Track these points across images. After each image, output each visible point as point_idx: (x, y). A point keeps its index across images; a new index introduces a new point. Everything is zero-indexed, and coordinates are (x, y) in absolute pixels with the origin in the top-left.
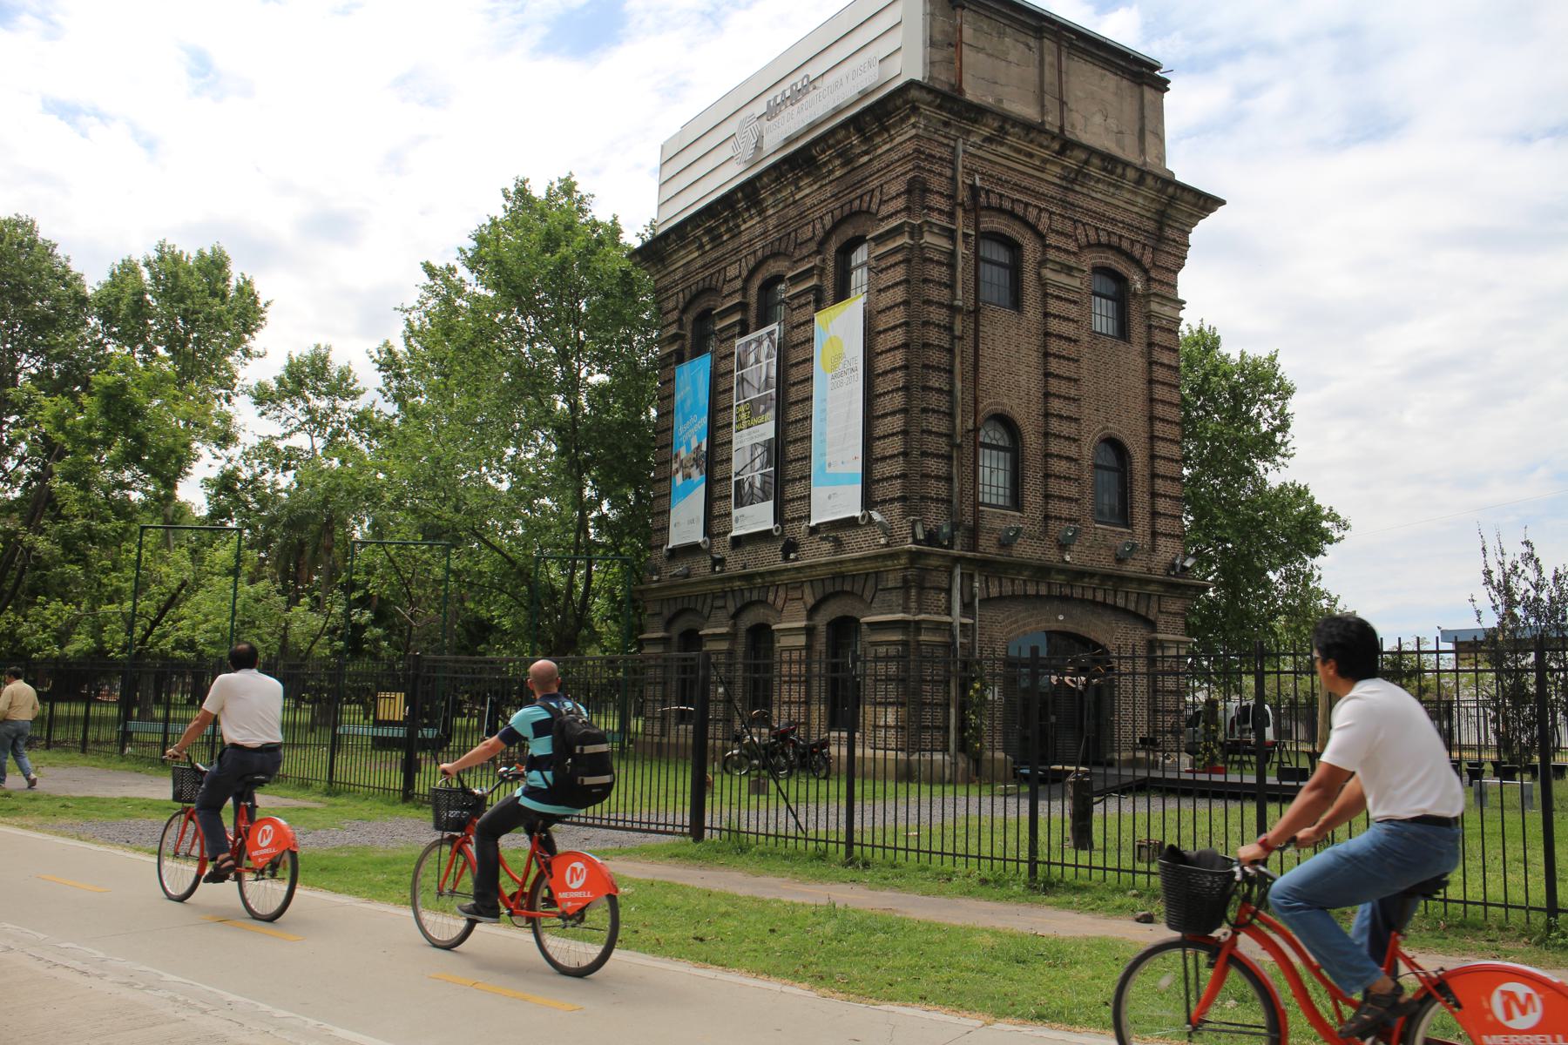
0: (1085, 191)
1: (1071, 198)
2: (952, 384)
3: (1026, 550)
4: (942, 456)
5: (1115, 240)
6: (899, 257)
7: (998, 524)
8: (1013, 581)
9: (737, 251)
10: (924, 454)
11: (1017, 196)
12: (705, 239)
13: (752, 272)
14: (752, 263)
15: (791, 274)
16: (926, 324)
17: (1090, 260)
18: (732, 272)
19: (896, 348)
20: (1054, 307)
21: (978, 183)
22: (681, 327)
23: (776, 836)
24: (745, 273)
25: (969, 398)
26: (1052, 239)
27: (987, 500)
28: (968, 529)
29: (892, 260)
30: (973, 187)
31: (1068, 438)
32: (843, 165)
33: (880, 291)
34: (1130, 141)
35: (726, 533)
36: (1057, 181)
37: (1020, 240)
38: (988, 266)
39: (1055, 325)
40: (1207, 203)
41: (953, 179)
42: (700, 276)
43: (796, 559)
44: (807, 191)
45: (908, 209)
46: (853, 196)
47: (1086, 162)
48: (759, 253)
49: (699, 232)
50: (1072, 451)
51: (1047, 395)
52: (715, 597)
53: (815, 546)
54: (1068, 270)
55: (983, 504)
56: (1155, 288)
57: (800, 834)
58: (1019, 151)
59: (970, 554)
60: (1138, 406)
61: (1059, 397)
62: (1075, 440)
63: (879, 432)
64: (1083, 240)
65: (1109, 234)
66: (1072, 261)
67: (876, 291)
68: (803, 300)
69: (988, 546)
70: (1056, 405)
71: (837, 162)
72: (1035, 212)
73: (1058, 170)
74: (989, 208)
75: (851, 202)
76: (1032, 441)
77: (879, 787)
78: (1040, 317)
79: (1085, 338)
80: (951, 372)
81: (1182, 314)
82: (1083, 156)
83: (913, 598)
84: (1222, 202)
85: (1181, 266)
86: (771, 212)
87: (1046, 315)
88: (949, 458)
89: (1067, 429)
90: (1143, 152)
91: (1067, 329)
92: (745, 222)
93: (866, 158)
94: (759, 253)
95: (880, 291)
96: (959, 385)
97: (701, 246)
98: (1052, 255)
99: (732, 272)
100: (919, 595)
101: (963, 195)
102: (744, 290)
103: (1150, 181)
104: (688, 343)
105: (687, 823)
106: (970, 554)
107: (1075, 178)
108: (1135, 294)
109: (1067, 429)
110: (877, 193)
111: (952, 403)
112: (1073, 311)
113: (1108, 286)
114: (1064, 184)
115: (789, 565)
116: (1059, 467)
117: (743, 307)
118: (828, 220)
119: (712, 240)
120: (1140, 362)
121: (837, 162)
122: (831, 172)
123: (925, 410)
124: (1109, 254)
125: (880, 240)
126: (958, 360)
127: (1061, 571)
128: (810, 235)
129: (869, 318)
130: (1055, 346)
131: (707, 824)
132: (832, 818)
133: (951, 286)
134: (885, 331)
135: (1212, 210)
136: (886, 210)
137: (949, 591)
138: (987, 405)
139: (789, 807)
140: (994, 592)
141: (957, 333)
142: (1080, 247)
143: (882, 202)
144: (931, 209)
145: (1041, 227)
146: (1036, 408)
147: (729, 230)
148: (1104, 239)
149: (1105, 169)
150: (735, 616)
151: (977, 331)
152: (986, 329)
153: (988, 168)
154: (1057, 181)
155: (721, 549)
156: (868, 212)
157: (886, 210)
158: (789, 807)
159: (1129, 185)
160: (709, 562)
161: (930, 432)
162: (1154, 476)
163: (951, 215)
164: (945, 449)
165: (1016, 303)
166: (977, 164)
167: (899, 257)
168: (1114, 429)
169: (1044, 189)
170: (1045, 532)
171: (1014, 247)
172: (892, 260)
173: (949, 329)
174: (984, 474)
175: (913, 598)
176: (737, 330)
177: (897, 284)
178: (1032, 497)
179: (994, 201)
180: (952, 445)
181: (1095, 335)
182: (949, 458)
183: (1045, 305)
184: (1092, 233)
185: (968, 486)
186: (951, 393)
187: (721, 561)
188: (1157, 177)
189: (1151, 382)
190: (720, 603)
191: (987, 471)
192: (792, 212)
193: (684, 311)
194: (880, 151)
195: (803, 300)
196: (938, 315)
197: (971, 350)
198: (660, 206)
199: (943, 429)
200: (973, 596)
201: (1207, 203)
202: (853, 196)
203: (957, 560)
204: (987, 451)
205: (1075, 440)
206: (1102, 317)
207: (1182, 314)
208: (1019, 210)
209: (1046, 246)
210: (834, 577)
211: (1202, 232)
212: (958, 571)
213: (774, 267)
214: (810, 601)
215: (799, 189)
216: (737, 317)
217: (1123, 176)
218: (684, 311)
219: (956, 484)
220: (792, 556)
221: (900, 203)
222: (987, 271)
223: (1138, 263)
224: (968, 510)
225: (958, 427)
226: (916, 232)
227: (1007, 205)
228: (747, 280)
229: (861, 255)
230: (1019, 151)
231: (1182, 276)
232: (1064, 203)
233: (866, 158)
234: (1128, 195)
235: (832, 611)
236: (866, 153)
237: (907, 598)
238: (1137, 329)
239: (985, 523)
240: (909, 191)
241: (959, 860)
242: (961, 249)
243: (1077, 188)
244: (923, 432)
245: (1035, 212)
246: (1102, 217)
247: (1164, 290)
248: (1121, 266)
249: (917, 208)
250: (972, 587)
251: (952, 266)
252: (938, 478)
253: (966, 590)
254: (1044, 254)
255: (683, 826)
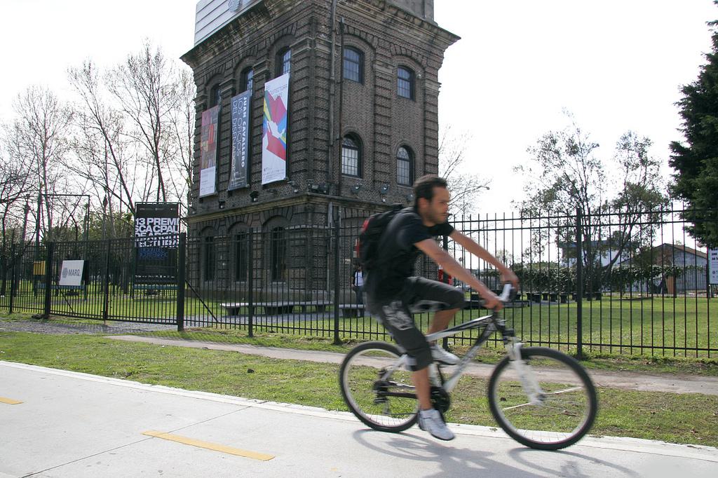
0: (395, 28)
1: (388, 31)
2: (329, 116)
3: (364, 197)
4: (324, 151)
5: (409, 53)
6: (304, 55)
7: (351, 183)
8: (358, 210)
9: (230, 55)
10: (315, 149)
11: (362, 29)
12: (216, 49)
13: (238, 65)
14: (237, 61)
15: (255, 65)
16: (317, 87)
17: (397, 61)
18: (229, 65)
19: (302, 99)
20: (379, 82)
21: (343, 21)
22: (205, 92)
23: (221, 323)
24: (234, 65)
25: (337, 124)
26: (379, 51)
27: (346, 172)
28: (336, 186)
29: (301, 57)
30: (340, 23)
31: (385, 144)
32: (280, 11)
33: (295, 72)
34: (418, 8)
35: (225, 190)
36: (382, 23)
37: (364, 50)
38: (348, 62)
39: (379, 91)
40: (453, 38)
41: (331, 19)
42: (213, 68)
43: (257, 201)
44: (263, 25)
45: (309, 32)
46: (284, 26)
47: (396, 15)
48: (241, 55)
49: (213, 46)
50: (387, 150)
51: (375, 124)
52: (221, 220)
53: (265, 194)
54: (386, 65)
55: (344, 174)
56: (428, 76)
57: (214, 321)
58: (364, 7)
59: (336, 197)
60: (419, 131)
61: (381, 125)
62: (388, 146)
63: (294, 139)
64: (394, 52)
65: (406, 49)
66: (388, 62)
67: (293, 73)
68: (260, 78)
69: (346, 194)
70: (379, 128)
71: (276, 10)
72: (371, 37)
73: (382, 18)
74: (349, 34)
75: (283, 30)
76: (368, 145)
77: (211, 289)
78: (372, 87)
79: (394, 98)
80: (328, 111)
81: (440, 89)
82: (394, 12)
83: (310, 218)
84: (460, 38)
85: (440, 67)
86: (246, 35)
87: (375, 86)
88: (327, 152)
89: (384, 140)
90: (423, 13)
91: (386, 93)
92: (234, 40)
93: (290, 8)
94: (241, 55)
95: (295, 72)
96: (332, 117)
97: (214, 53)
98: (378, 58)
99: (229, 65)
100: (312, 216)
101: (336, 27)
102: (234, 73)
103: (426, 25)
104: (209, 100)
105: (175, 319)
106: (336, 197)
107: (392, 21)
108: (418, 79)
109: (384, 140)
110: (295, 25)
111: (329, 126)
112: (388, 85)
113: (405, 75)
114: (385, 24)
115: (253, 204)
116: (380, 157)
117: (233, 81)
118: (272, 38)
119: (219, 50)
120: (420, 111)
121: (276, 10)
122: (274, 15)
123: (315, 129)
124: (407, 59)
125: (296, 47)
126: (332, 105)
127: (380, 206)
128: (264, 46)
129: (291, 84)
130: (379, 101)
131: (185, 319)
132: (189, 309)
133: (329, 70)
134: (297, 91)
135: (454, 42)
136: (298, 33)
137: (326, 214)
138: (346, 128)
139: (209, 311)
140: (349, 215)
141: (332, 92)
142: (392, 55)
143: (297, 29)
144: (320, 33)
145: (373, 45)
146: (370, 130)
147: (227, 45)
148: (404, 52)
149: (405, 19)
150: (229, 230)
151: (341, 92)
152: (346, 92)
153: (348, 14)
154: (382, 23)
155: (224, 197)
156: (291, 34)
157: (298, 33)
158: (209, 311)
159: (416, 27)
160: (218, 204)
161: (318, 139)
162: (425, 163)
163: (330, 36)
164: (325, 148)
165: (361, 80)
166: (343, 12)
167: (304, 55)
168: (408, 141)
169: (375, 26)
170: (374, 188)
171: (361, 53)
172: (301, 57)
173: (328, 90)
174: (344, 160)
175: (310, 218)
176: (231, 93)
177: (303, 68)
178: (368, 171)
179: (351, 31)
180: (329, 146)
181: (399, 97)
182: (327, 152)
183: (375, 81)
184: (398, 49)
185: (336, 165)
186: (328, 121)
187: (222, 203)
188: (429, 24)
189: (425, 120)
190: (222, 223)
191: (346, 159)
192: (256, 35)
193: (207, 85)
194: (296, 5)
195: (260, 78)
196: (323, 84)
197: (339, 101)
198: (196, 34)
199: (324, 138)
200: (338, 217)
201: (453, 38)
202: (284, 26)
203: (330, 199)
204: (346, 150)
205: (388, 146)
206: (403, 88)
207: (440, 89)
208: (363, 35)
209: (375, 54)
210: (274, 208)
211: (450, 53)
212: (331, 205)
213: (248, 62)
214: (263, 221)
215: (259, 24)
216: (230, 87)
217: (413, 23)
218: (207, 85)
219: (330, 164)
220: (255, 200)
221: (305, 30)
222: (347, 64)
223: (420, 64)
224: (336, 177)
225: (332, 137)
226: (313, 43)
227: (357, 33)
228: (235, 69)
229: (288, 56)
230: (364, 7)
231: (440, 72)
232: (385, 34)
233: (290, 8)
234: (415, 32)
235: (274, 224)
236: (290, 5)
237: (307, 217)
238: (419, 95)
239: (345, 183)
240: (310, 24)
241: (219, 325)
242: (334, 53)
243: (391, 27)
244: (315, 139)
245: (371, 37)
246: (403, 42)
247: (432, 78)
248: (412, 65)
249: (314, 33)
250: (338, 213)
251: (330, 60)
252: (322, 161)
253: (335, 214)
254: (375, 57)
255: (100, 316)
